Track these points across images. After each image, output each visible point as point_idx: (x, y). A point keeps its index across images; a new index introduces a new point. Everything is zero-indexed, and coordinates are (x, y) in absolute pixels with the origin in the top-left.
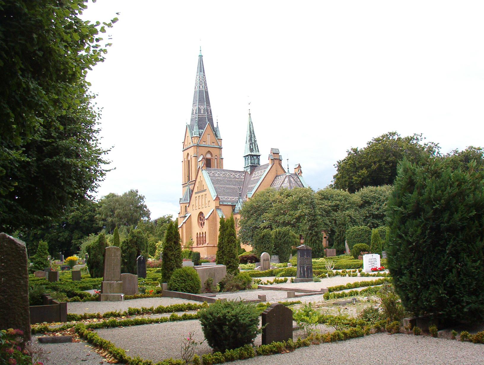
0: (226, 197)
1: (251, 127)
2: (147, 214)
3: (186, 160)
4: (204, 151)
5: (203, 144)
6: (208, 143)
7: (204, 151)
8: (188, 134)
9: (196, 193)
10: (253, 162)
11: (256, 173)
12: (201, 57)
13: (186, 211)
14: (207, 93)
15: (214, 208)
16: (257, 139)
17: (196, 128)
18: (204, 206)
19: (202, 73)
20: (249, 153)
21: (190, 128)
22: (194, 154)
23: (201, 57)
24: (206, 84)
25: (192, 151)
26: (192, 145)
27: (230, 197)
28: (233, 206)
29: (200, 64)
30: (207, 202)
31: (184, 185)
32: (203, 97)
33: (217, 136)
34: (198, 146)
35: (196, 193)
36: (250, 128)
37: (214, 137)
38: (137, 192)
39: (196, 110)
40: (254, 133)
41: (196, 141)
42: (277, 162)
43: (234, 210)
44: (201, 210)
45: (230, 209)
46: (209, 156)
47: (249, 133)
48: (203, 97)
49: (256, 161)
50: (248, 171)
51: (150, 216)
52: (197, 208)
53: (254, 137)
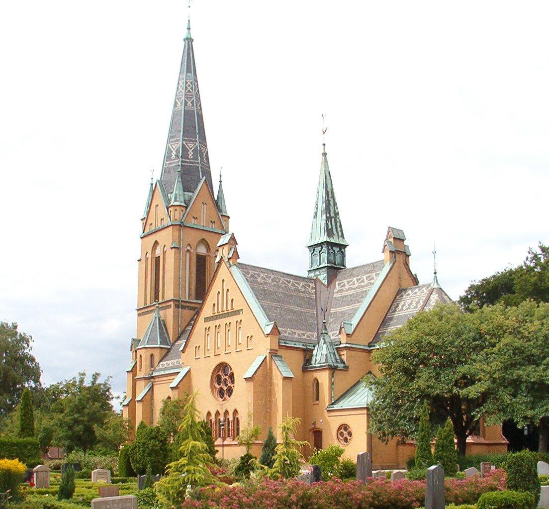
0: (289, 331)
1: (329, 182)
2: (34, 373)
3: (149, 256)
4: (193, 237)
5: (192, 223)
6: (203, 223)
7: (193, 237)
8: (159, 199)
9: (207, 319)
10: (332, 258)
11: (344, 286)
12: (189, 41)
13: (152, 365)
14: (200, 117)
15: (266, 353)
16: (341, 210)
17: (177, 192)
18: (232, 349)
19: (192, 75)
20: (324, 238)
21: (161, 187)
22: (173, 241)
23: (189, 41)
24: (198, 100)
25: (166, 238)
26: (167, 222)
27: (297, 332)
28: (308, 354)
29: (189, 55)
30: (242, 339)
31: (142, 311)
32: (190, 124)
33: (221, 211)
34: (181, 226)
35: (207, 319)
36: (326, 185)
37: (213, 210)
38: (15, 327)
39: (178, 151)
40: (333, 197)
41: (177, 215)
42: (400, 258)
43: (308, 361)
44: (223, 359)
45: (298, 358)
46: (202, 250)
47: (323, 194)
48: (190, 124)
49: (338, 260)
50: (321, 277)
51: (41, 380)
52: (212, 355)
53: (335, 204)
